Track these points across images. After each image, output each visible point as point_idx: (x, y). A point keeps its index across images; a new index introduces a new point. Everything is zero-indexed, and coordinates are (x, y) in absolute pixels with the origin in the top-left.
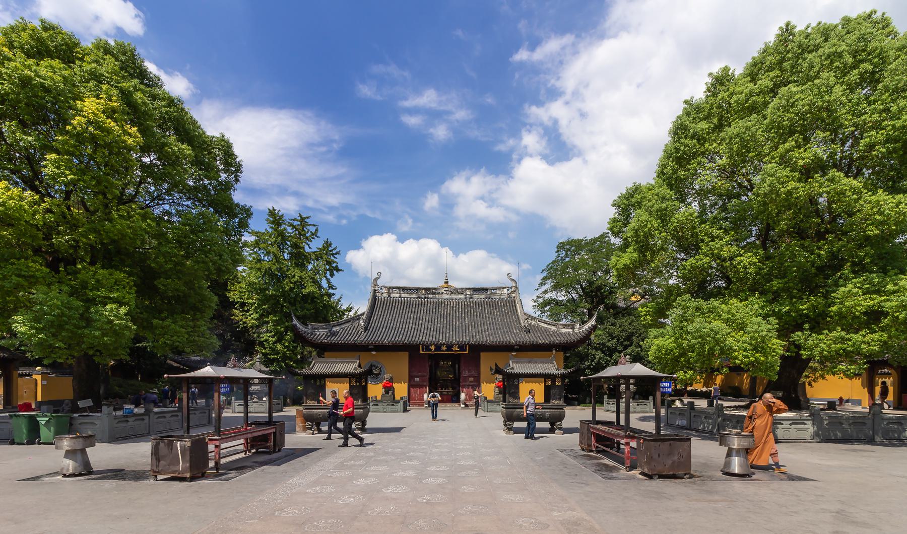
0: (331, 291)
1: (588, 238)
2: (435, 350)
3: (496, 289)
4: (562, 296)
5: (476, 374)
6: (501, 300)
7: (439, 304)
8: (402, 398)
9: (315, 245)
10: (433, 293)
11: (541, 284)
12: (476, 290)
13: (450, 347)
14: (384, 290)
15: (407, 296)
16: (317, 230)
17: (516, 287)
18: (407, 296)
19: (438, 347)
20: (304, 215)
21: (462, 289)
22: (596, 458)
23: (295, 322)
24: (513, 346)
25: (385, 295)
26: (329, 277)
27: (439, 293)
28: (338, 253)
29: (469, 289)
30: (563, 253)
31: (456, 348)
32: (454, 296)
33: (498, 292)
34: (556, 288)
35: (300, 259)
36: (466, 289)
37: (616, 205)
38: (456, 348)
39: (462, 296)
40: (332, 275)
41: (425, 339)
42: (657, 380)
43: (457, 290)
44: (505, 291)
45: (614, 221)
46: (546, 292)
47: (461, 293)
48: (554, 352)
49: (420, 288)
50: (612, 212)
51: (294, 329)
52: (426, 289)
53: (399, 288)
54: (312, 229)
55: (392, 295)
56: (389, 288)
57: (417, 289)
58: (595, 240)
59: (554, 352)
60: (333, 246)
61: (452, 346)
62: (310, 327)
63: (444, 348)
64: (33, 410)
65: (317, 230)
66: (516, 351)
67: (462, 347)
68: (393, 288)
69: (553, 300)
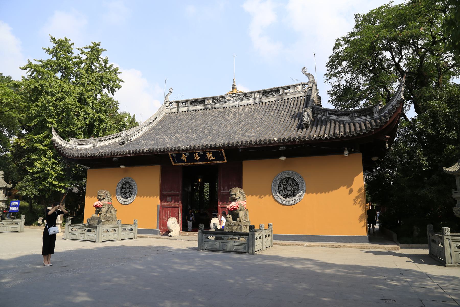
2: (200, 160)
3: (288, 88)
8: (385, 56)
10: (220, 102)
12: (266, 93)
14: (174, 105)
17: (314, 83)
21: (250, 93)
22: (429, 236)
23: (55, 137)
25: (175, 110)
27: (225, 101)
29: (258, 92)
36: (255, 92)
38: (209, 156)
39: (250, 101)
42: (54, 128)
43: (245, 94)
44: (300, 88)
47: (248, 98)
48: (346, 153)
49: (207, 98)
51: (53, 146)
52: (213, 99)
55: (181, 110)
56: (178, 103)
64: (185, 162)
67: (215, 150)
68: (183, 102)
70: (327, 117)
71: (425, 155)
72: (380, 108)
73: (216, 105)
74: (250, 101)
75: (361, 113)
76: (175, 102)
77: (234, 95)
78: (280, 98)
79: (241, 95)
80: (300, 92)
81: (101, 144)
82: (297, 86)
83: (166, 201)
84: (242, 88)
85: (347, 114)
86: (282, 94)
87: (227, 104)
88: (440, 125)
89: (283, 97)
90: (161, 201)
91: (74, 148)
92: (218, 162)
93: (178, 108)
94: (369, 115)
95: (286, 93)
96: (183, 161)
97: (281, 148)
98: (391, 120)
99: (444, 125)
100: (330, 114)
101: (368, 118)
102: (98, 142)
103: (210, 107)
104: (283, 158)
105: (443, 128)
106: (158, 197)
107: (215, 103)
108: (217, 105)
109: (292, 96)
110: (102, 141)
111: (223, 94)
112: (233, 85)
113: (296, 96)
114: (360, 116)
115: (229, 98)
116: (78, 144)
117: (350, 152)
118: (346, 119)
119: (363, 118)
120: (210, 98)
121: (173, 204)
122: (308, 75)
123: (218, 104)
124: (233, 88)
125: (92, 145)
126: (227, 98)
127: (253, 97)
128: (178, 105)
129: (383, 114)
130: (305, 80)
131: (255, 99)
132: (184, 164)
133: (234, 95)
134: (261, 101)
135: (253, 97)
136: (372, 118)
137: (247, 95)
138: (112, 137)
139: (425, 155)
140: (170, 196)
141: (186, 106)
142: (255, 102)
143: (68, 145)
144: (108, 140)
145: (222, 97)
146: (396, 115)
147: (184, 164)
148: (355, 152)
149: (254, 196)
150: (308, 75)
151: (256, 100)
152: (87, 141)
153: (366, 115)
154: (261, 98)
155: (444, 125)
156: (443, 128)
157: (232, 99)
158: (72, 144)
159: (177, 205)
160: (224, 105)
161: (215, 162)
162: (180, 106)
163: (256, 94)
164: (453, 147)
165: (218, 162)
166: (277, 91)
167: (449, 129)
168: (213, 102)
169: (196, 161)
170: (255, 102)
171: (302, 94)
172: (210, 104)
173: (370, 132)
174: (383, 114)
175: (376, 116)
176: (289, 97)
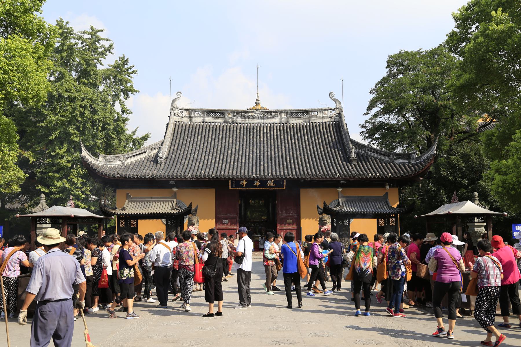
0: (125, 116)
1: (424, 50)
2: (247, 185)
3: (316, 111)
4: (393, 120)
5: (295, 215)
6: (323, 125)
7: (249, 130)
9: (105, 64)
10: (243, 117)
11: (370, 107)
12: (293, 113)
13: (263, 182)
14: (185, 114)
15: (212, 120)
16: (111, 46)
18: (212, 120)
19: (250, 182)
20: (97, 28)
21: (276, 112)
23: (85, 153)
24: (339, 181)
25: (186, 119)
26: (123, 99)
27: (248, 117)
28: (134, 72)
29: (285, 111)
30: (395, 69)
31: (270, 183)
32: (267, 121)
33: (319, 114)
34: (386, 111)
35: (85, 74)
36: (281, 112)
37: (456, 19)
38: (270, 183)
39: (276, 120)
40: (127, 96)
41: (236, 172)
43: (270, 112)
44: (328, 113)
45: (452, 35)
46: (376, 116)
47: (274, 116)
48: (387, 187)
49: (227, 111)
50: (451, 26)
51: (84, 163)
52: (234, 112)
53: (202, 111)
54: (107, 44)
55: (194, 119)
56: (190, 111)
57: (223, 113)
58: (433, 52)
59: (387, 187)
60: (129, 64)
61: (267, 182)
62: (101, 159)
63: (257, 183)
65: (111, 46)
66: (342, 186)
67: (278, 182)
68: (195, 111)
69: (385, 124)
70: (366, 153)
71: (446, 194)
72: (416, 156)
73: (238, 119)
74: (276, 120)
75: (400, 156)
76: (186, 110)
77: (258, 112)
78: (307, 120)
79: (267, 112)
80: (327, 118)
81: (129, 161)
82: (325, 110)
83: (222, 223)
84: (268, 104)
85: (386, 155)
86: (310, 117)
87: (250, 120)
88: (457, 174)
89: (311, 120)
90: (216, 223)
91: (105, 166)
92: (277, 188)
93: (191, 117)
94: (407, 159)
95: (313, 117)
96: (241, 186)
97: (342, 182)
98: (426, 167)
99: (460, 175)
100: (368, 150)
101: (406, 162)
102: (127, 158)
103: (230, 121)
104: (340, 189)
105: (459, 177)
106: (214, 220)
107: (237, 118)
108: (239, 120)
109: (320, 121)
110: (130, 157)
111: (245, 108)
112: (257, 100)
113: (324, 121)
114: (399, 158)
115: (253, 114)
116: (107, 160)
117: (390, 187)
118: (385, 158)
119: (401, 161)
120: (231, 111)
121: (230, 227)
122: (336, 101)
123: (241, 119)
124: (257, 104)
125: (120, 162)
126: (251, 114)
127: (279, 117)
128: (190, 114)
129: (419, 161)
130: (333, 105)
131: (281, 118)
132: (241, 189)
133: (258, 112)
134: (288, 122)
135: (279, 117)
136: (410, 162)
137: (273, 114)
138: (138, 153)
139: (446, 194)
140: (226, 219)
141: (201, 117)
142: (281, 122)
143: (98, 162)
144: (135, 156)
145: (245, 112)
146: (429, 164)
147: (241, 189)
148: (393, 186)
149: (311, 219)
150: (336, 101)
151: (283, 119)
152: (116, 157)
153: (404, 159)
154: (288, 119)
155: (460, 175)
156: (459, 177)
157: (256, 115)
158: (102, 161)
159: (235, 227)
160: (247, 121)
161: (274, 188)
162: (192, 115)
163: (283, 114)
164: (464, 191)
165: (277, 188)
166: (304, 112)
167: (463, 178)
168: (234, 116)
169: (255, 187)
170: (281, 122)
171: (329, 120)
172: (231, 118)
173: (411, 175)
174: (419, 161)
175: (413, 161)
176: (317, 121)
